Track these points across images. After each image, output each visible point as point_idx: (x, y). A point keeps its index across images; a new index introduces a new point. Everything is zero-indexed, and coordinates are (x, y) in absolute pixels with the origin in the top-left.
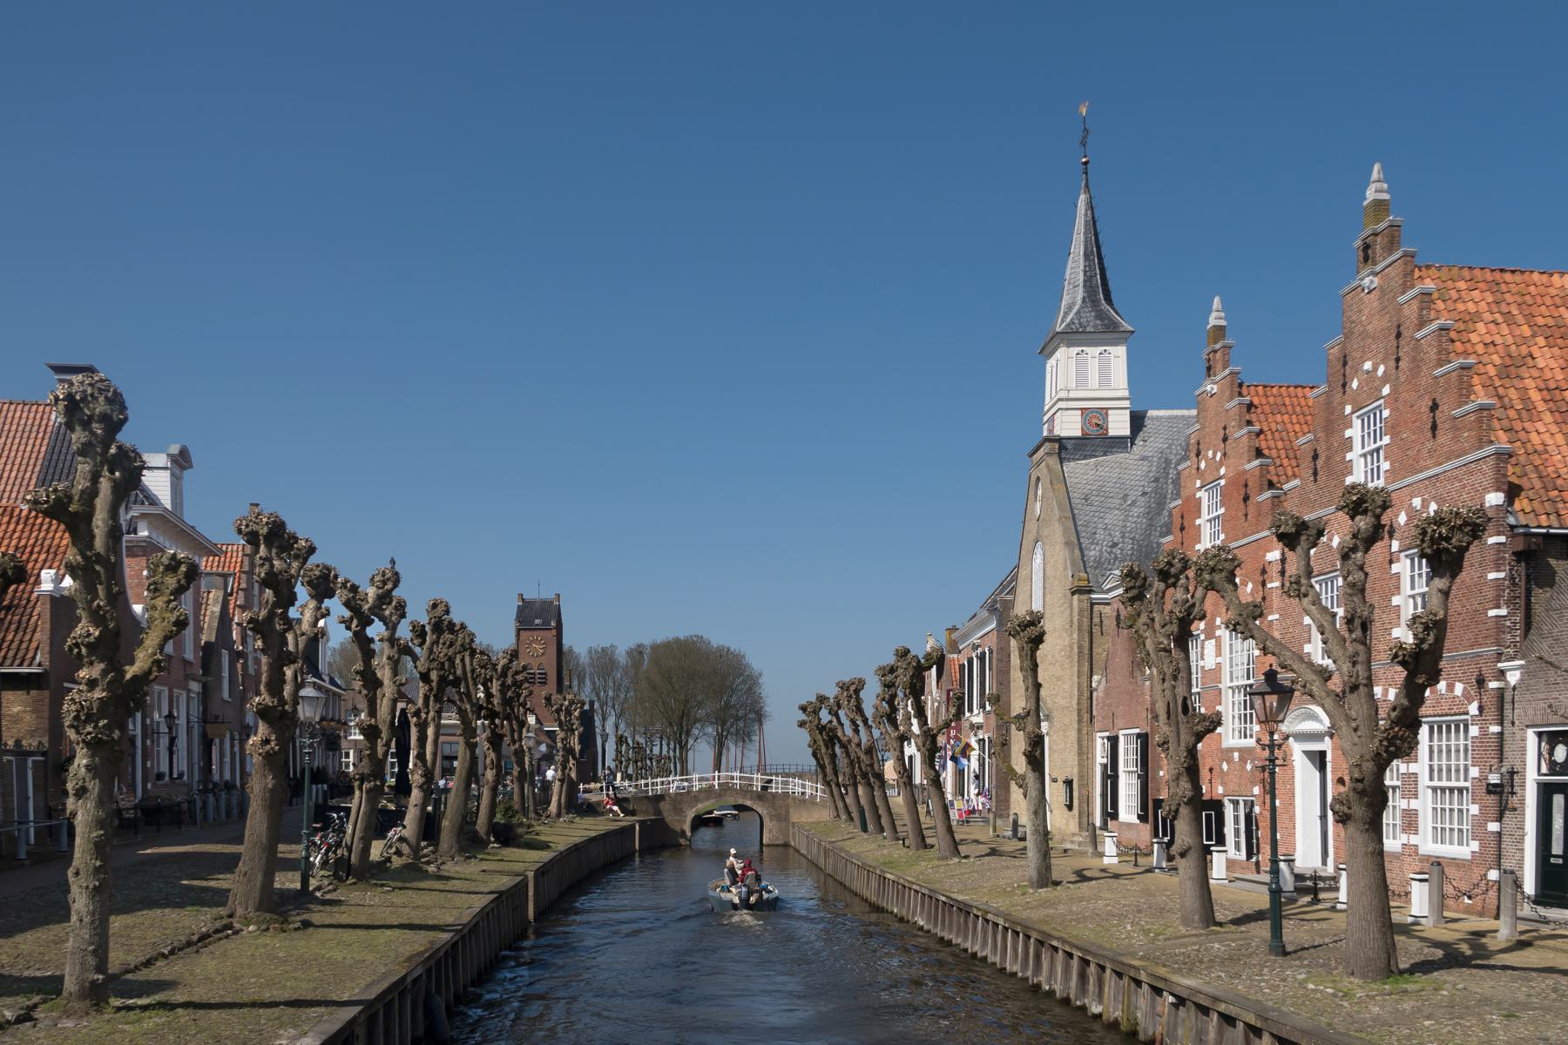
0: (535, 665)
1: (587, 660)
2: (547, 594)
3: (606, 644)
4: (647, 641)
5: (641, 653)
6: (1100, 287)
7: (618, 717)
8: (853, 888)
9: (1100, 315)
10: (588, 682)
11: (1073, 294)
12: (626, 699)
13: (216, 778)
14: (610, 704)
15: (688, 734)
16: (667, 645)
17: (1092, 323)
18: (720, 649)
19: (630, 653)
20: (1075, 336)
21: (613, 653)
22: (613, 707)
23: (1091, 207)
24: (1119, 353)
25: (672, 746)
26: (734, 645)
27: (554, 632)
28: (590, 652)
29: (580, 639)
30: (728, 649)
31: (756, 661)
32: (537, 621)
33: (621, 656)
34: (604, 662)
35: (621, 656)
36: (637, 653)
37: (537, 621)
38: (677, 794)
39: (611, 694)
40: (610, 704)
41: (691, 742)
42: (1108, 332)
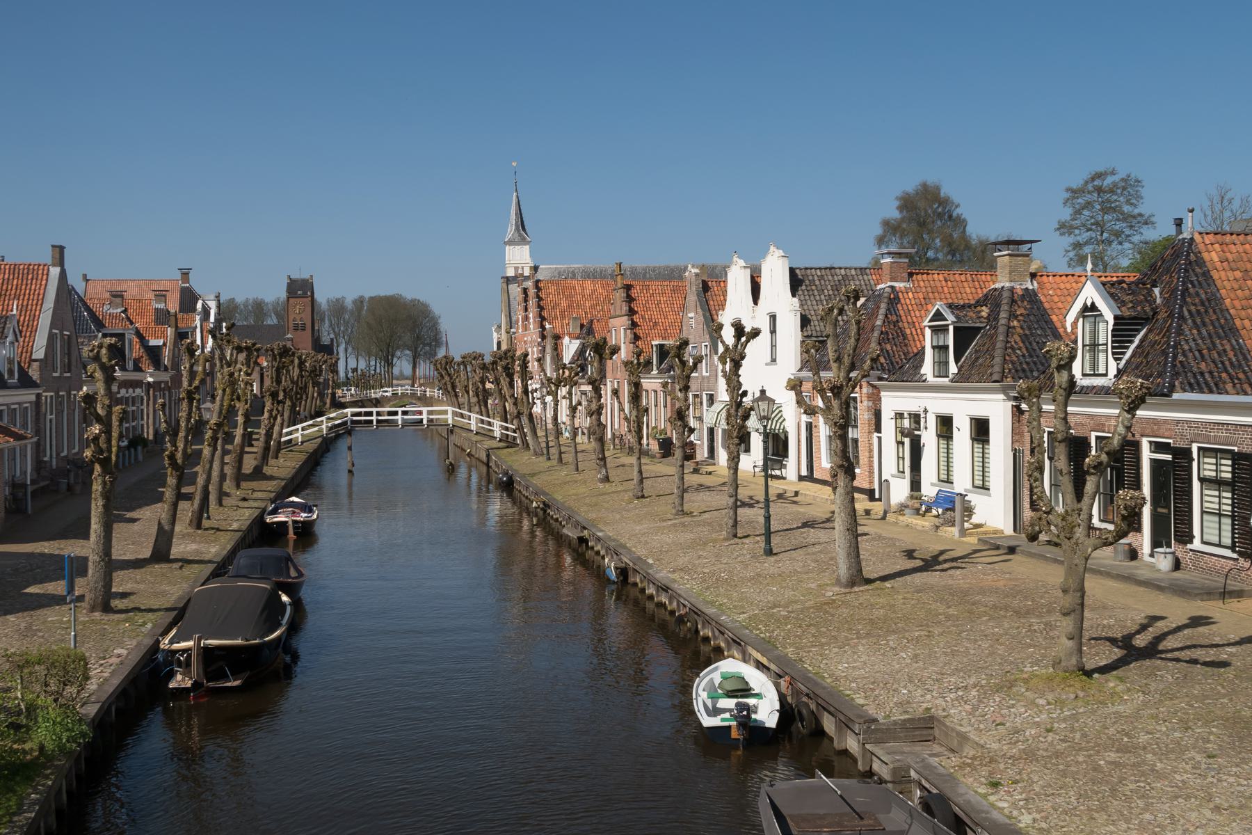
0: (298, 318)
1: (327, 307)
2: (305, 276)
3: (339, 296)
4: (368, 294)
5: (362, 302)
6: (521, 225)
7: (347, 343)
8: (860, 546)
9: (520, 235)
10: (327, 321)
11: (511, 231)
12: (352, 332)
13: (1230, 514)
14: (342, 335)
15: (393, 356)
16: (376, 301)
17: (517, 238)
18: (413, 301)
19: (355, 302)
20: (511, 243)
21: (343, 302)
22: (344, 337)
23: (518, 197)
24: (527, 247)
25: (382, 364)
26: (422, 296)
27: (310, 299)
28: (328, 302)
29: (323, 295)
30: (419, 301)
31: (436, 308)
32: (299, 292)
33: (349, 303)
34: (338, 307)
35: (349, 303)
36: (359, 302)
37: (299, 292)
38: (331, 428)
39: (342, 328)
40: (342, 335)
41: (395, 360)
42: (523, 241)
